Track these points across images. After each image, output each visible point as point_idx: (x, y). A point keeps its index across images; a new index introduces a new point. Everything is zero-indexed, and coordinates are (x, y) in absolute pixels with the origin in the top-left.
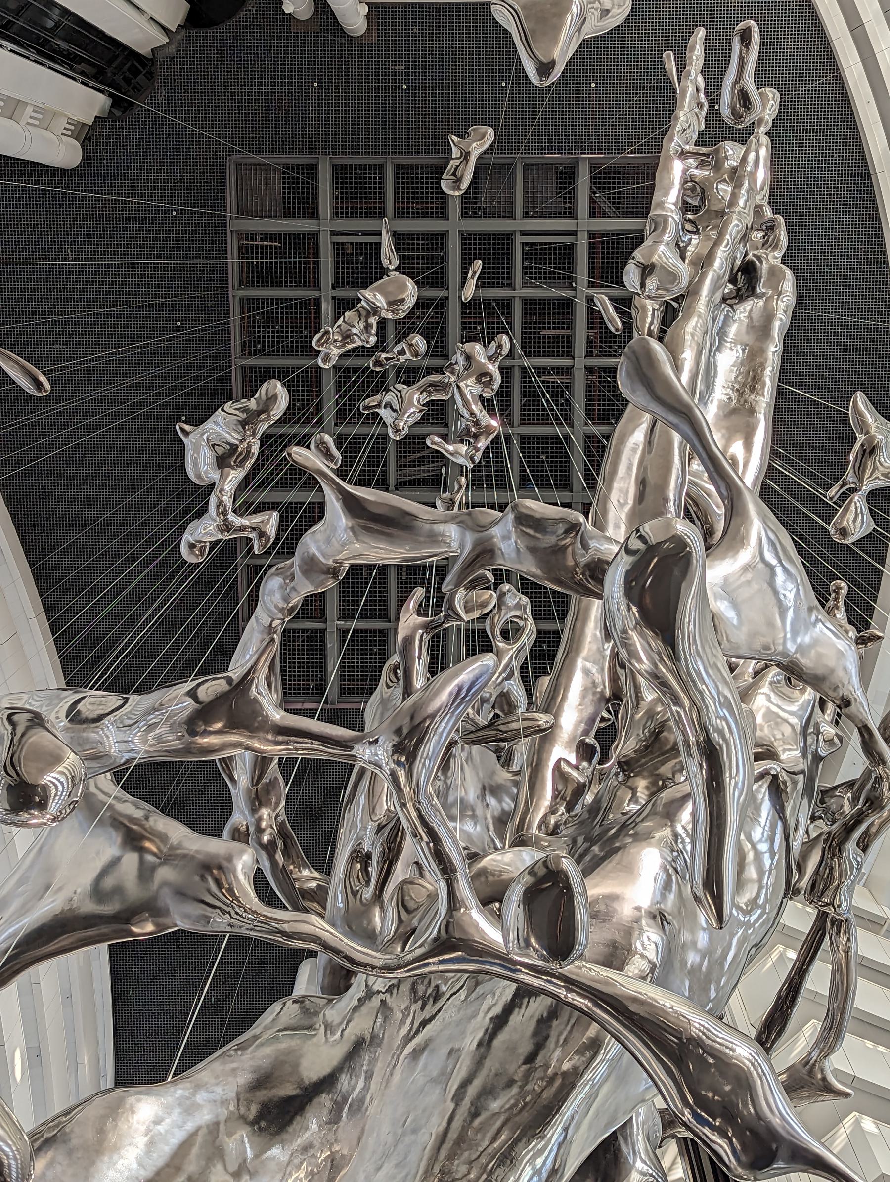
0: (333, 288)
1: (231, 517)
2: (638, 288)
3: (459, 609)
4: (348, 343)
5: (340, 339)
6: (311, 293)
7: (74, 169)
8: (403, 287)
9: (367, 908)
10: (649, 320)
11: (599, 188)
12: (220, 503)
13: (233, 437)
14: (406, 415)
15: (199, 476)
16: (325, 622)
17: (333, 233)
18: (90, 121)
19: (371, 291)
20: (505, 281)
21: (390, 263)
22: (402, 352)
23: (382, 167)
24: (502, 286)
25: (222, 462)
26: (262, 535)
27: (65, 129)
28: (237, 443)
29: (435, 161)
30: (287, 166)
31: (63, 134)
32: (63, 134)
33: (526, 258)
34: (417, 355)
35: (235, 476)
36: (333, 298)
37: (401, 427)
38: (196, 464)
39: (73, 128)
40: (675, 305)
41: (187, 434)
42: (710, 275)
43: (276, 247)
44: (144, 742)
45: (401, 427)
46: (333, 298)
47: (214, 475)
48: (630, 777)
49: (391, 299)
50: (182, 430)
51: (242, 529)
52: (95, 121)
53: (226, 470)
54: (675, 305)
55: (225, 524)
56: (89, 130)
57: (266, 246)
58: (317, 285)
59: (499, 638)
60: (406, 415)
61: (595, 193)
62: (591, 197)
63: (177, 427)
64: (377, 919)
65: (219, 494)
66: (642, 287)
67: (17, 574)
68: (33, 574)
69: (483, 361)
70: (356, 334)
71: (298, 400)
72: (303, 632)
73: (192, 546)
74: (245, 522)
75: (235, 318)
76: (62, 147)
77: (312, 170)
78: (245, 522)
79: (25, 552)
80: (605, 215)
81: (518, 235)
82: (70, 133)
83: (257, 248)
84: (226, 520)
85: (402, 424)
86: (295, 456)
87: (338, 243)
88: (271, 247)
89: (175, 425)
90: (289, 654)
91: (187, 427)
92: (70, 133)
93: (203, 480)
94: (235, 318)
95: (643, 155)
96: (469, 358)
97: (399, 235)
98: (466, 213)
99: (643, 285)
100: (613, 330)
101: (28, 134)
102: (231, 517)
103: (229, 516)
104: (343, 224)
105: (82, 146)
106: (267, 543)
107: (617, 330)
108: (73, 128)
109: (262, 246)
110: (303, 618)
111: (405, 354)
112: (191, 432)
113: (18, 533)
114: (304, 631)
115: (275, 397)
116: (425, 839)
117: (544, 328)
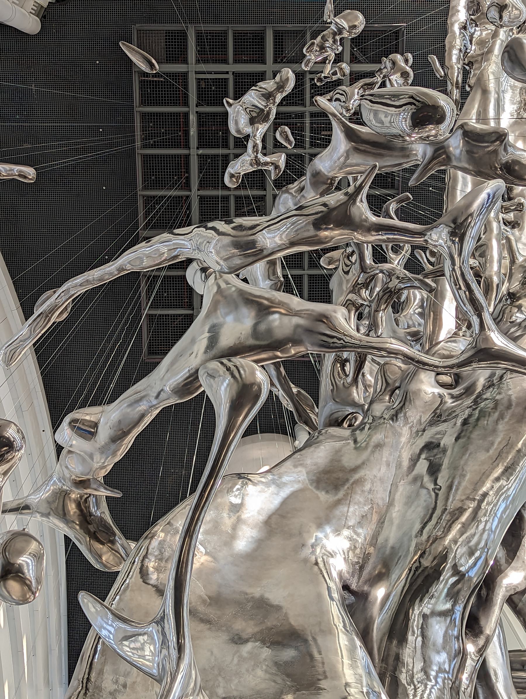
0: (197, 106)
1: (260, 156)
2: (498, 19)
3: (392, 214)
4: (324, 53)
5: (318, 50)
6: (184, 109)
7: (36, 35)
8: (357, 18)
9: (347, 388)
10: (456, 74)
11: (356, 46)
12: (255, 146)
13: (261, 103)
14: (353, 101)
15: (238, 131)
16: (193, 309)
17: (197, 73)
18: (45, 5)
19: (339, 18)
20: (300, 102)
21: (329, 18)
22: (335, 73)
23: (226, 33)
24: (299, 105)
25: (252, 121)
26: (277, 167)
27: (32, 9)
28: (263, 108)
29: (138, 117)
30: (168, 32)
31: (30, 12)
32: (30, 12)
33: (313, 88)
34: (344, 75)
35: (262, 128)
36: (197, 112)
37: (351, 108)
38: (236, 123)
39: (36, 9)
40: (467, 68)
41: (230, 105)
42: (498, 42)
43: (162, 81)
44: (281, 239)
45: (351, 108)
46: (197, 112)
47: (248, 130)
48: (514, 302)
49: (351, 24)
50: (227, 102)
51: (266, 164)
52: (49, 5)
53: (256, 125)
54: (467, 68)
55: (255, 160)
56: (45, 11)
57: (156, 81)
58: (186, 104)
59: (390, 251)
60: (353, 101)
61: (353, 48)
62: (351, 51)
63: (224, 101)
64: (355, 394)
65: (254, 139)
66: (500, 19)
67: (5, 283)
68: (14, 284)
69: (403, 65)
70: (328, 47)
71: (176, 175)
72: (179, 316)
73: (232, 176)
74: (268, 159)
75: (138, 124)
76: (31, 19)
77: (183, 35)
78: (268, 159)
79: (9, 271)
80: (359, 62)
81: (308, 73)
82: (34, 12)
83: (147, 82)
84: (256, 157)
85: (351, 106)
86: (319, 102)
87: (199, 79)
88: (159, 81)
89: (223, 100)
90: (171, 330)
91: (231, 101)
92: (34, 12)
93: (241, 134)
94: (138, 124)
95: (384, 25)
96: (394, 63)
97: (236, 74)
98: (276, 60)
99: (501, 17)
100: (438, 76)
101: (14, 8)
102: (260, 156)
103: (259, 155)
104: (203, 67)
105: (41, 21)
106: (279, 172)
107: (441, 77)
108: (36, 9)
109: (153, 81)
110: (179, 308)
111: (337, 74)
112: (233, 104)
113: (4, 259)
114: (180, 315)
115: (287, 79)
116: (463, 288)
117: (324, 130)
